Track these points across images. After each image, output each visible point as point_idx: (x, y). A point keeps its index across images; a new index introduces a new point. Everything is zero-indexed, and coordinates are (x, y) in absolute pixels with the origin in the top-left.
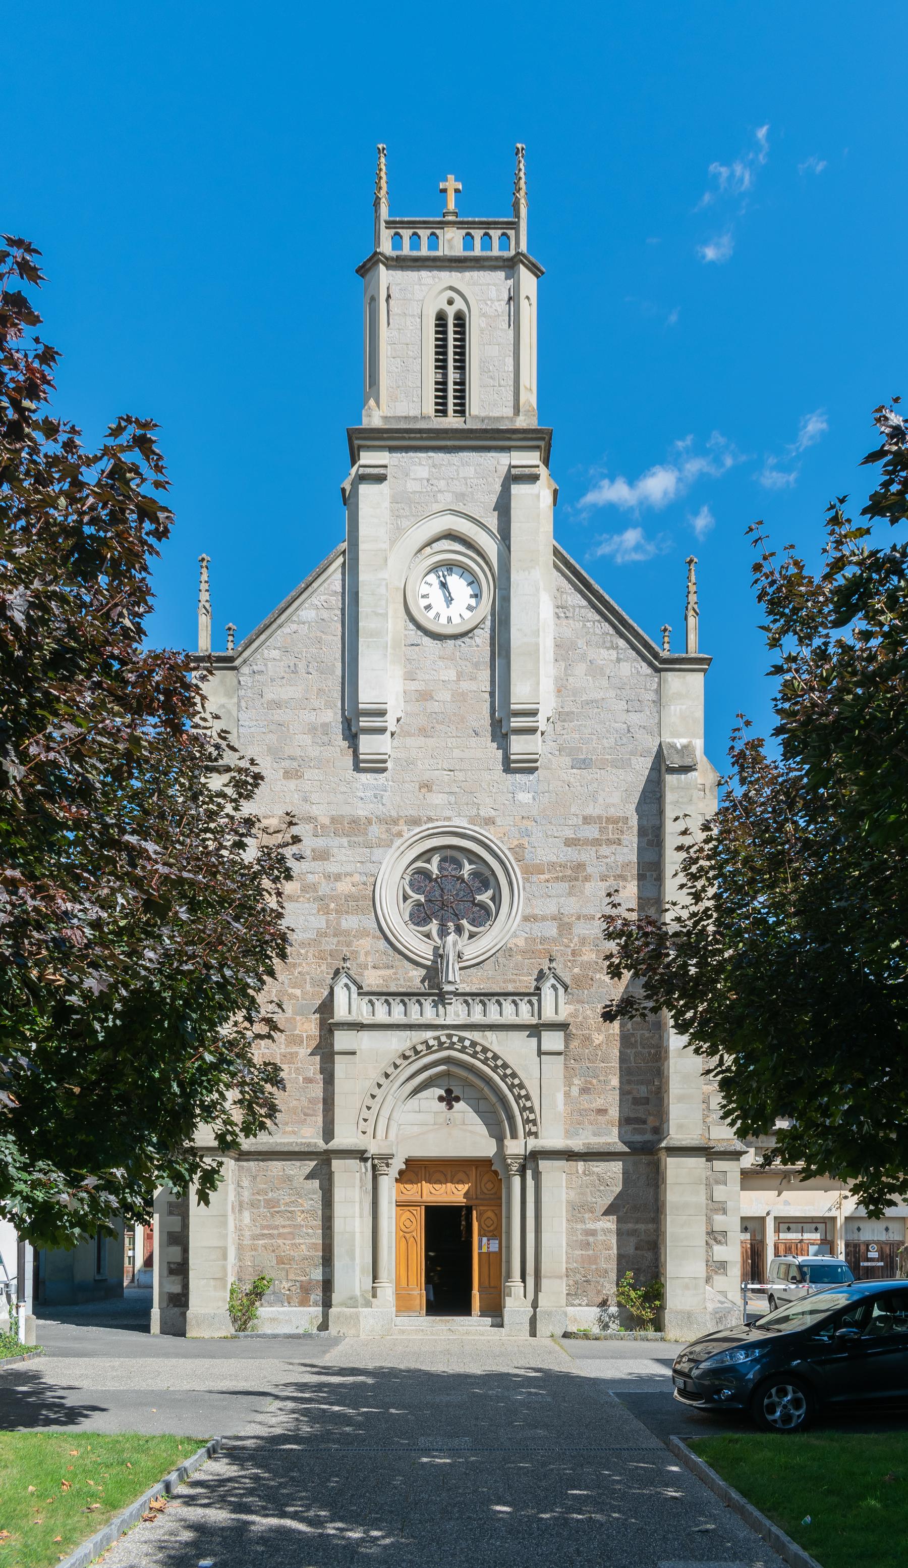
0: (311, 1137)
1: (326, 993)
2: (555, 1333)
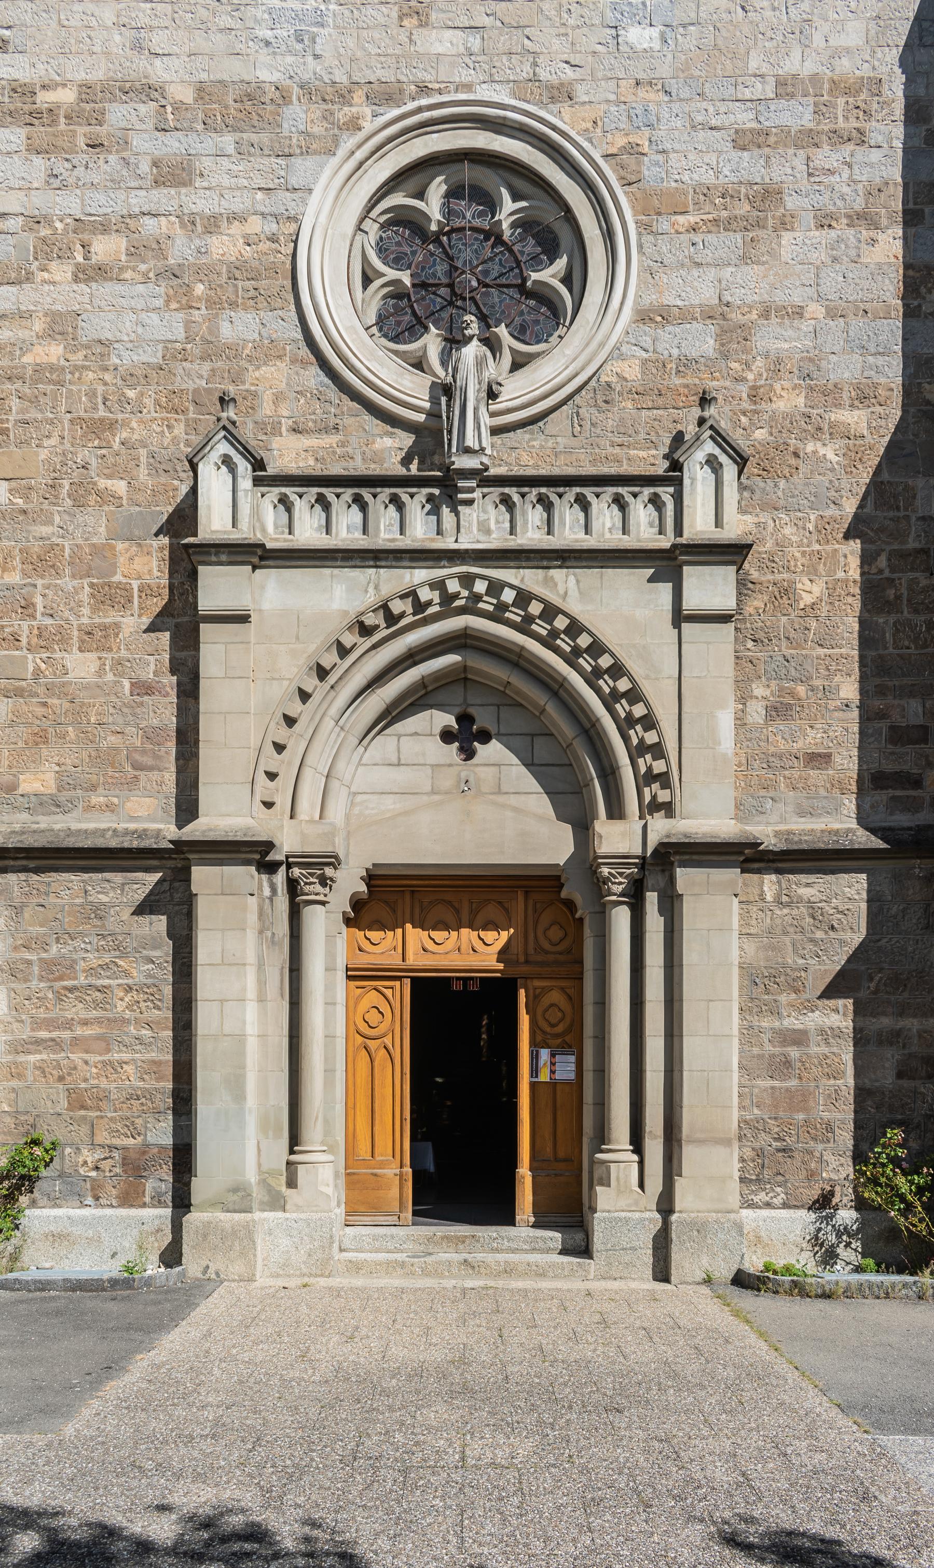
0: (154, 820)
1: (184, 489)
2: (716, 1275)
